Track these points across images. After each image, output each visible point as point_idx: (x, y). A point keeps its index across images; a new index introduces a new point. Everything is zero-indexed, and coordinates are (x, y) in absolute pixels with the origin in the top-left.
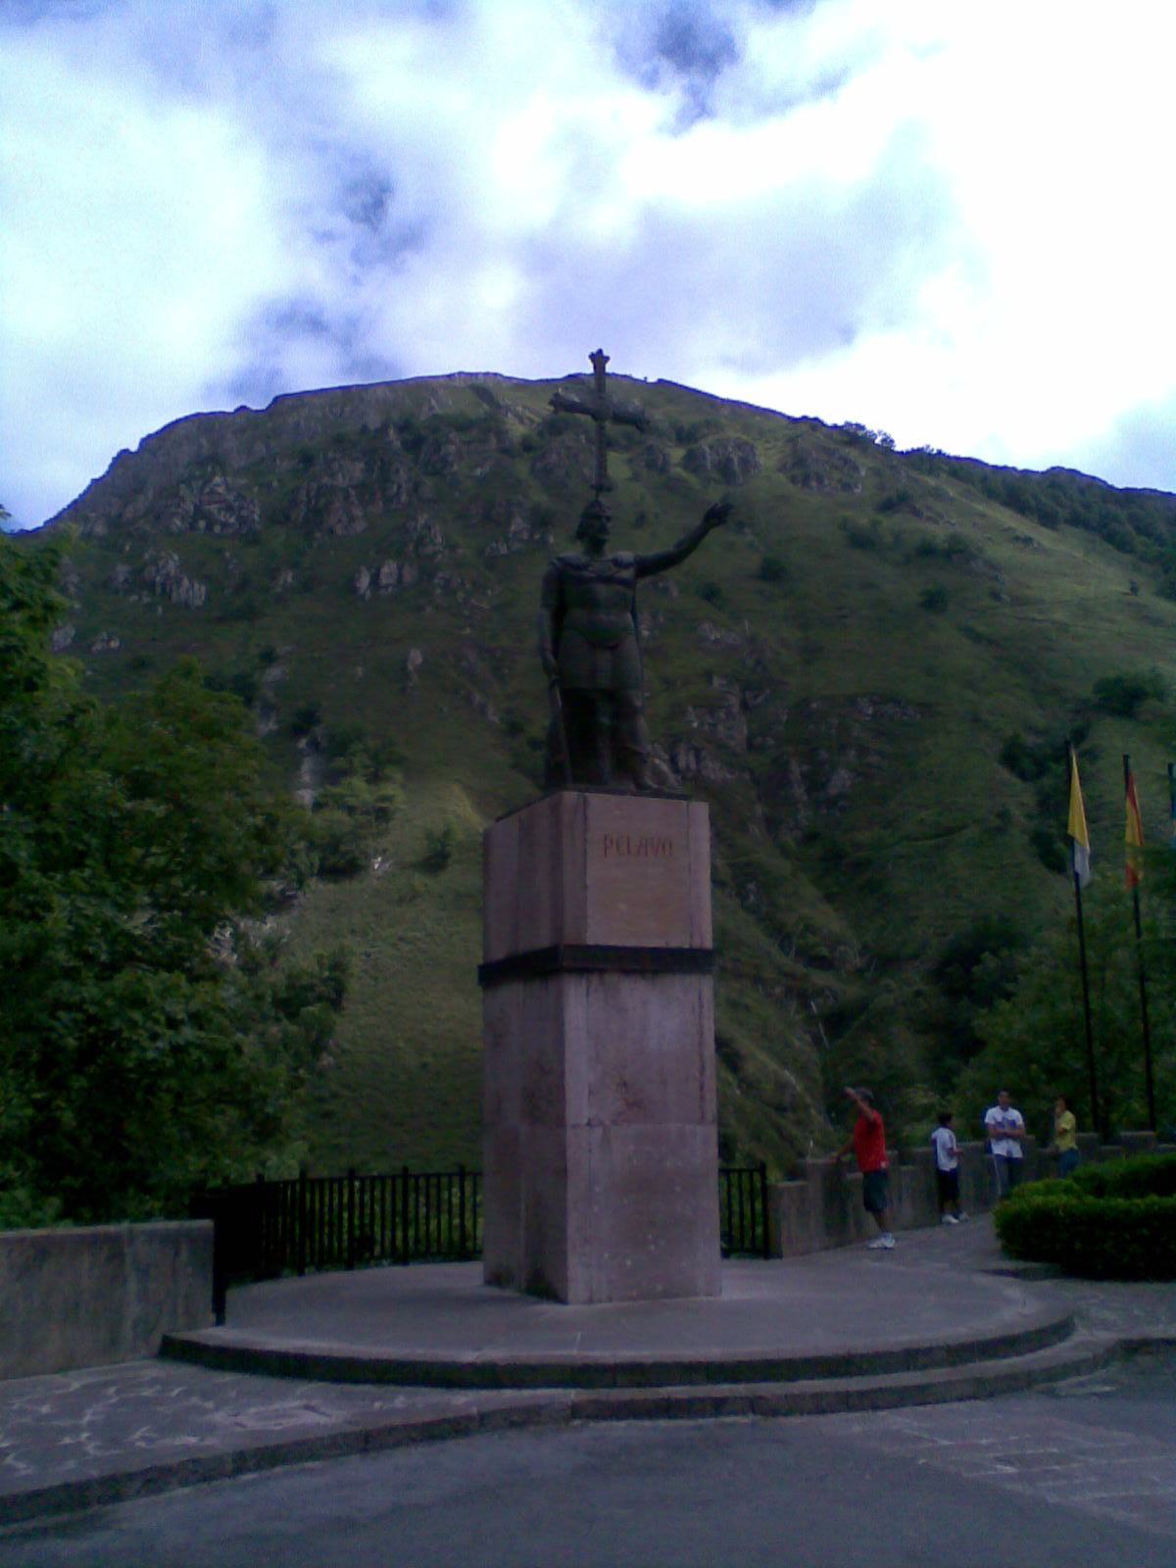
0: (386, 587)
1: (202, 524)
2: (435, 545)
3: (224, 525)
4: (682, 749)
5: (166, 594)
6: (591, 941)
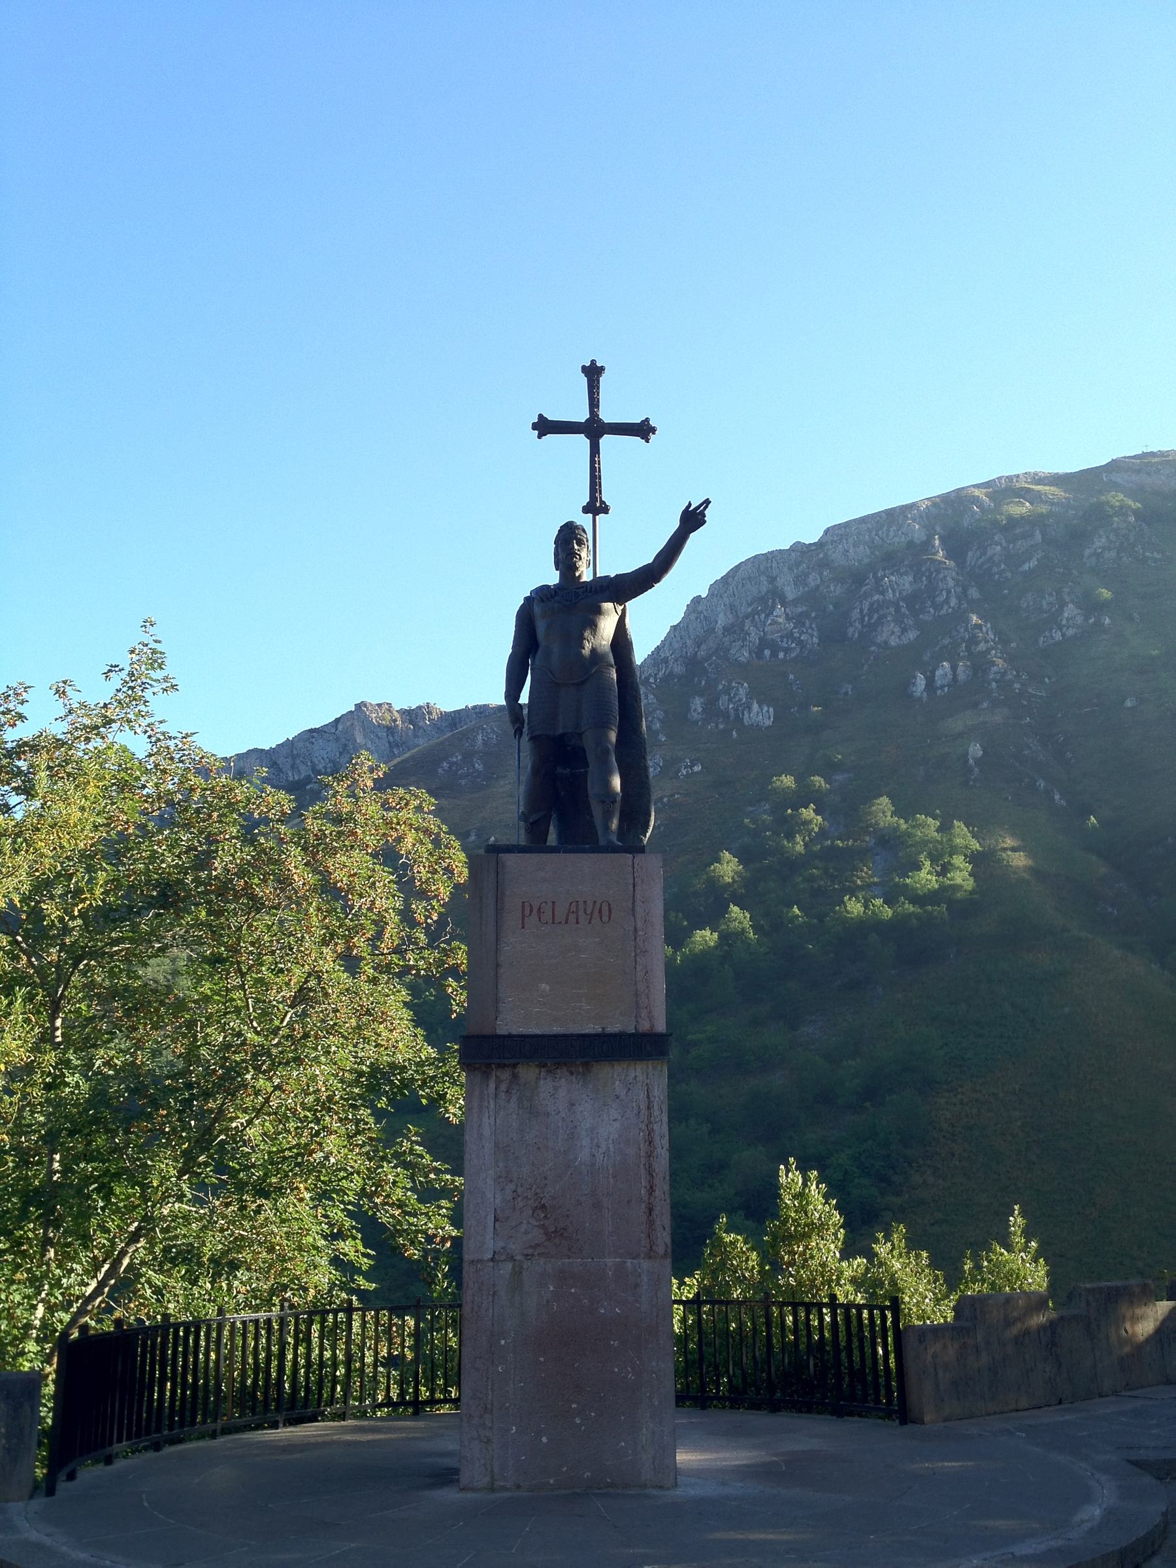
0: (942, 687)
1: (767, 653)
3: (787, 650)
5: (739, 719)
6: (502, 1030)
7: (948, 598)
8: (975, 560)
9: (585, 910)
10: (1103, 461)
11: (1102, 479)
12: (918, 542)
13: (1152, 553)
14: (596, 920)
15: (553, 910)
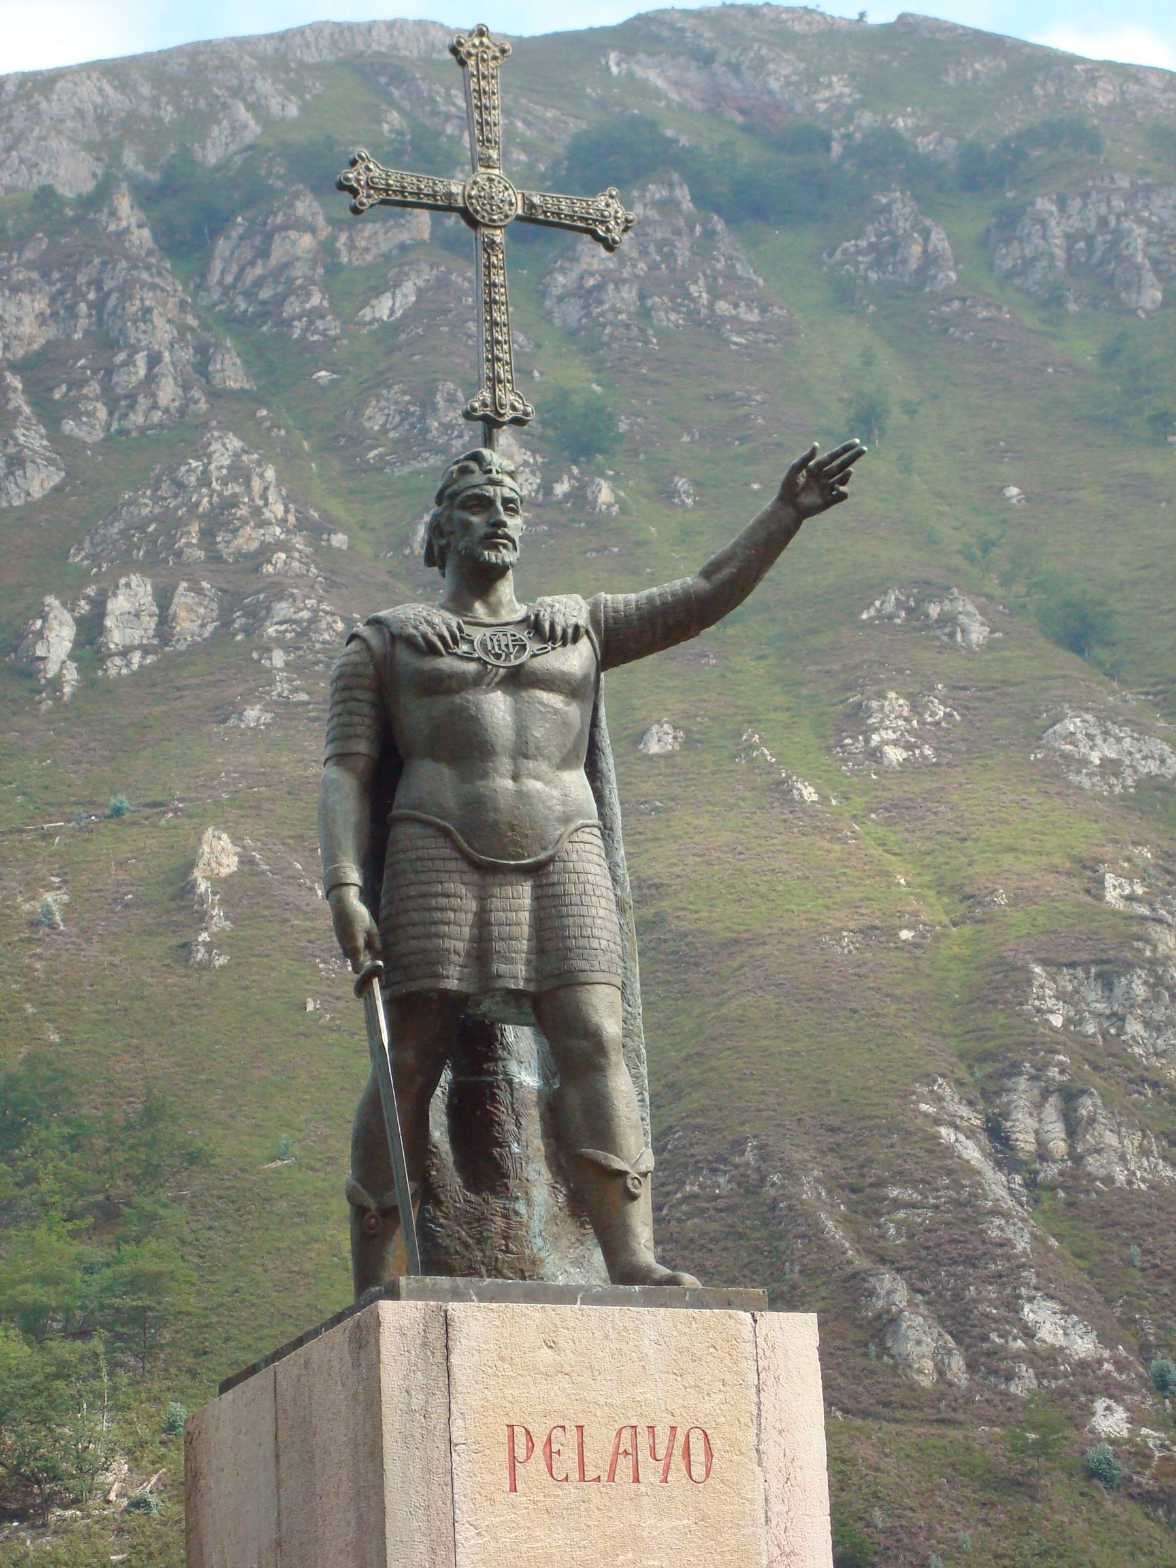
0: (125, 652)
2: (263, 524)
4: (1022, 1092)
7: (151, 379)
8: (235, 268)
9: (653, 1449)
10: (613, 16)
11: (608, 68)
12: (69, 195)
13: (736, 306)
14: (677, 1474)
15: (581, 1445)
